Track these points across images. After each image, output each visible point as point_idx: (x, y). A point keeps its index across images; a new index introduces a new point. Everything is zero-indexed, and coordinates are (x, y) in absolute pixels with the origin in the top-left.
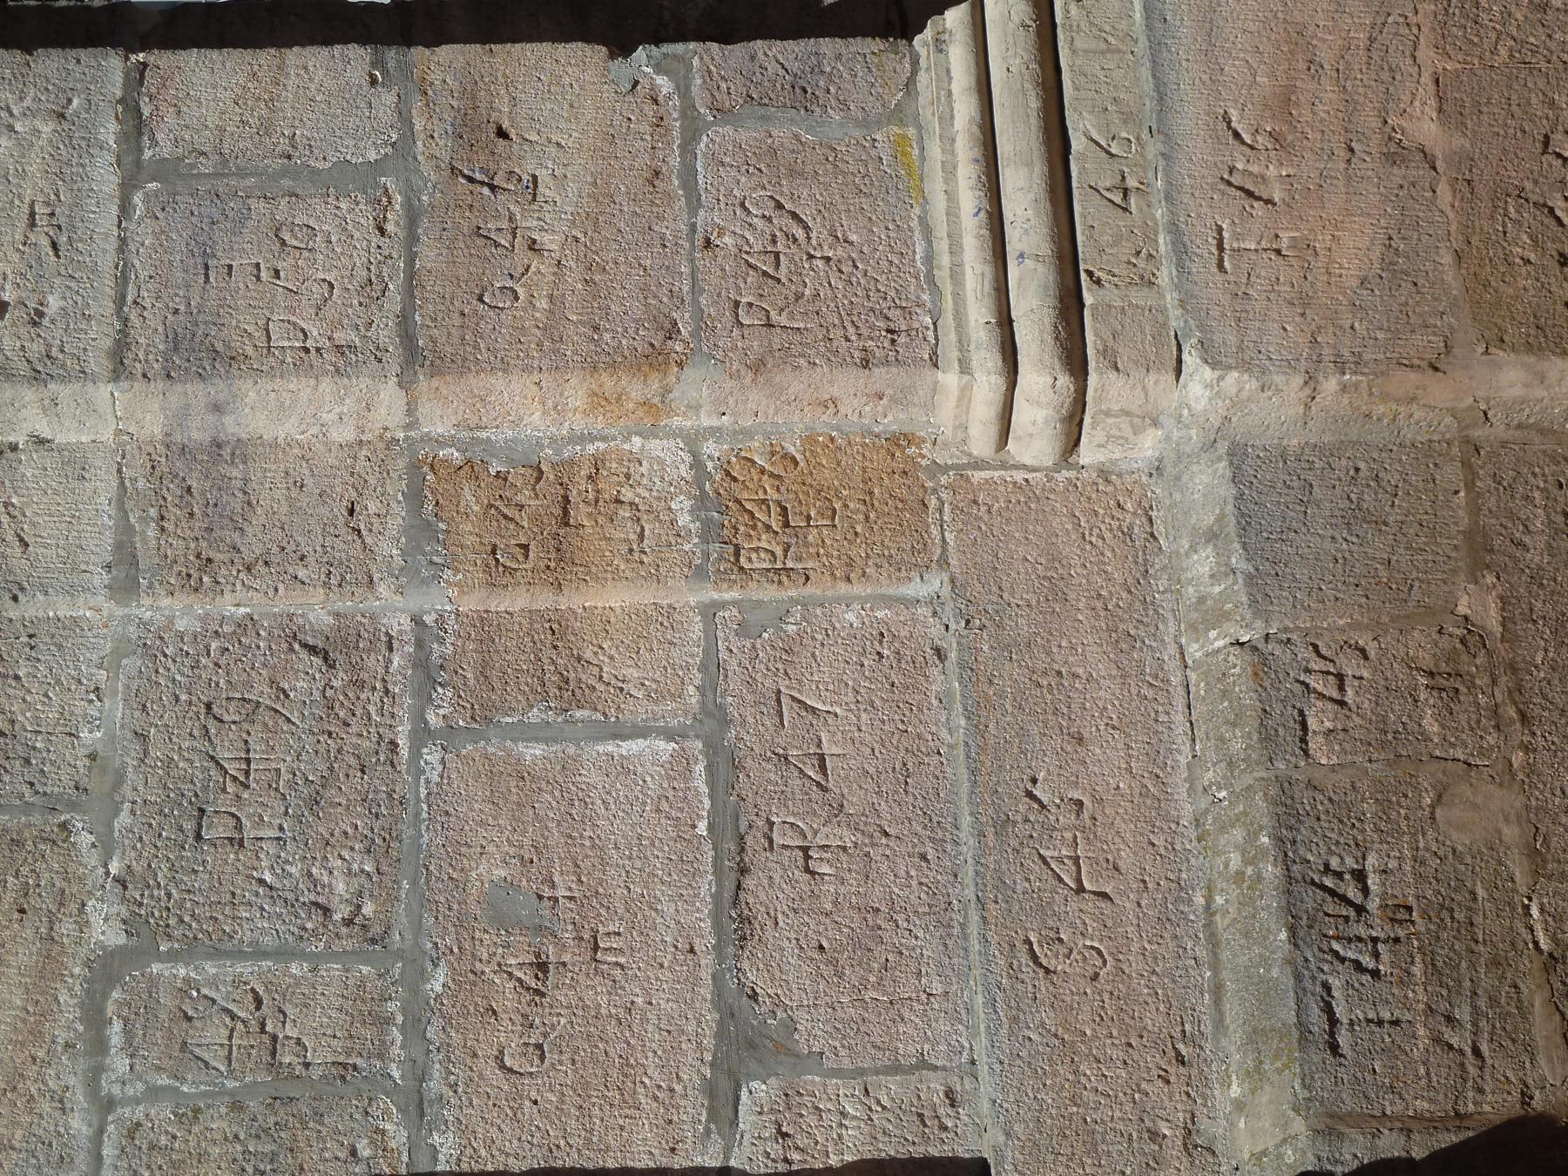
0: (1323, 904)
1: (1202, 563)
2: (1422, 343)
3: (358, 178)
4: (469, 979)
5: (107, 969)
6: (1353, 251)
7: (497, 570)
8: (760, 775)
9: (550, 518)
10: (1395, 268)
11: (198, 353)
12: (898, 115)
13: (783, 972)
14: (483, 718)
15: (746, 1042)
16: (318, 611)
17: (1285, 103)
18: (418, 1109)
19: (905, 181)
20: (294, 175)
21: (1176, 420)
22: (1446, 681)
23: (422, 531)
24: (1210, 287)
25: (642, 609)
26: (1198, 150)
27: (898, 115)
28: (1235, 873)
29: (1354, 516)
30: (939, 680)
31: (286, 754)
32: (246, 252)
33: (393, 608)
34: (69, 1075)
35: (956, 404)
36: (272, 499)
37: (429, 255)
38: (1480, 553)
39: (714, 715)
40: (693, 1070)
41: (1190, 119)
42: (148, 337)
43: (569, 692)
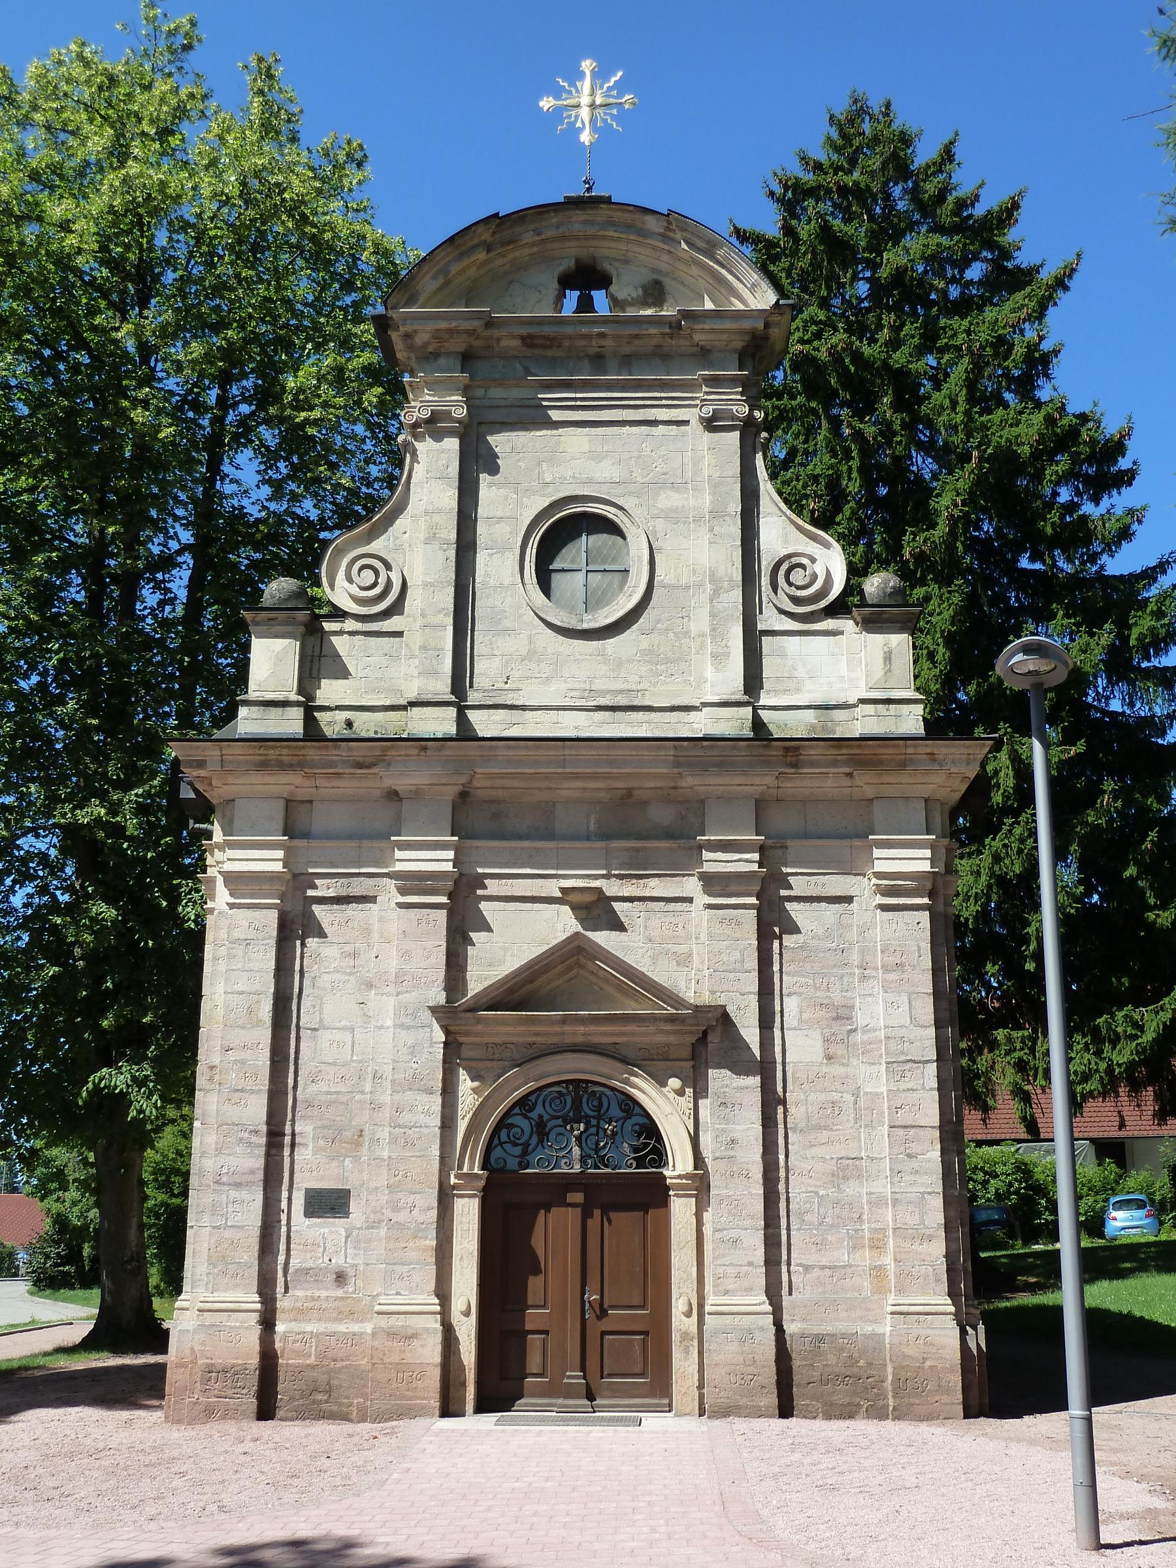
0: (820, 1338)
1: (870, 1329)
2: (894, 1358)
3: (923, 1222)
4: (815, 1235)
5: (817, 1193)
6: (908, 1351)
7: (870, 1239)
8: (843, 1271)
9: (878, 1246)
10: (905, 1356)
11: (895, 1202)
12: (935, 1293)
13: (816, 1273)
14: (851, 1237)
15: (807, 1268)
16: (865, 1217)
17: (931, 1344)
18: (799, 1229)
19: (924, 1294)
20: (922, 1214)
21: (886, 1328)
22: (851, 1357)
23: (876, 1230)
24: (903, 1332)
25: (865, 1258)
26: (923, 1332)
27: (935, 1293)
28: (828, 1329)
29: (875, 1349)
30: (856, 1295)
31: (845, 1213)
32: (911, 1208)
33: (865, 1226)
34: (803, 1189)
35: (892, 1299)
36: (880, 1211)
37: (910, 1231)
38: (870, 1365)
39: (851, 1266)
40: (804, 1262)
41: (929, 1332)
42: (897, 1196)
43: (854, 1248)
